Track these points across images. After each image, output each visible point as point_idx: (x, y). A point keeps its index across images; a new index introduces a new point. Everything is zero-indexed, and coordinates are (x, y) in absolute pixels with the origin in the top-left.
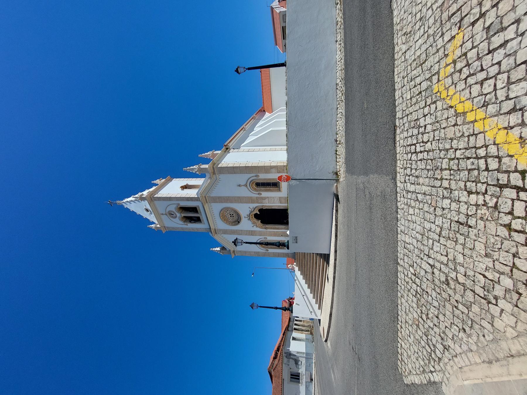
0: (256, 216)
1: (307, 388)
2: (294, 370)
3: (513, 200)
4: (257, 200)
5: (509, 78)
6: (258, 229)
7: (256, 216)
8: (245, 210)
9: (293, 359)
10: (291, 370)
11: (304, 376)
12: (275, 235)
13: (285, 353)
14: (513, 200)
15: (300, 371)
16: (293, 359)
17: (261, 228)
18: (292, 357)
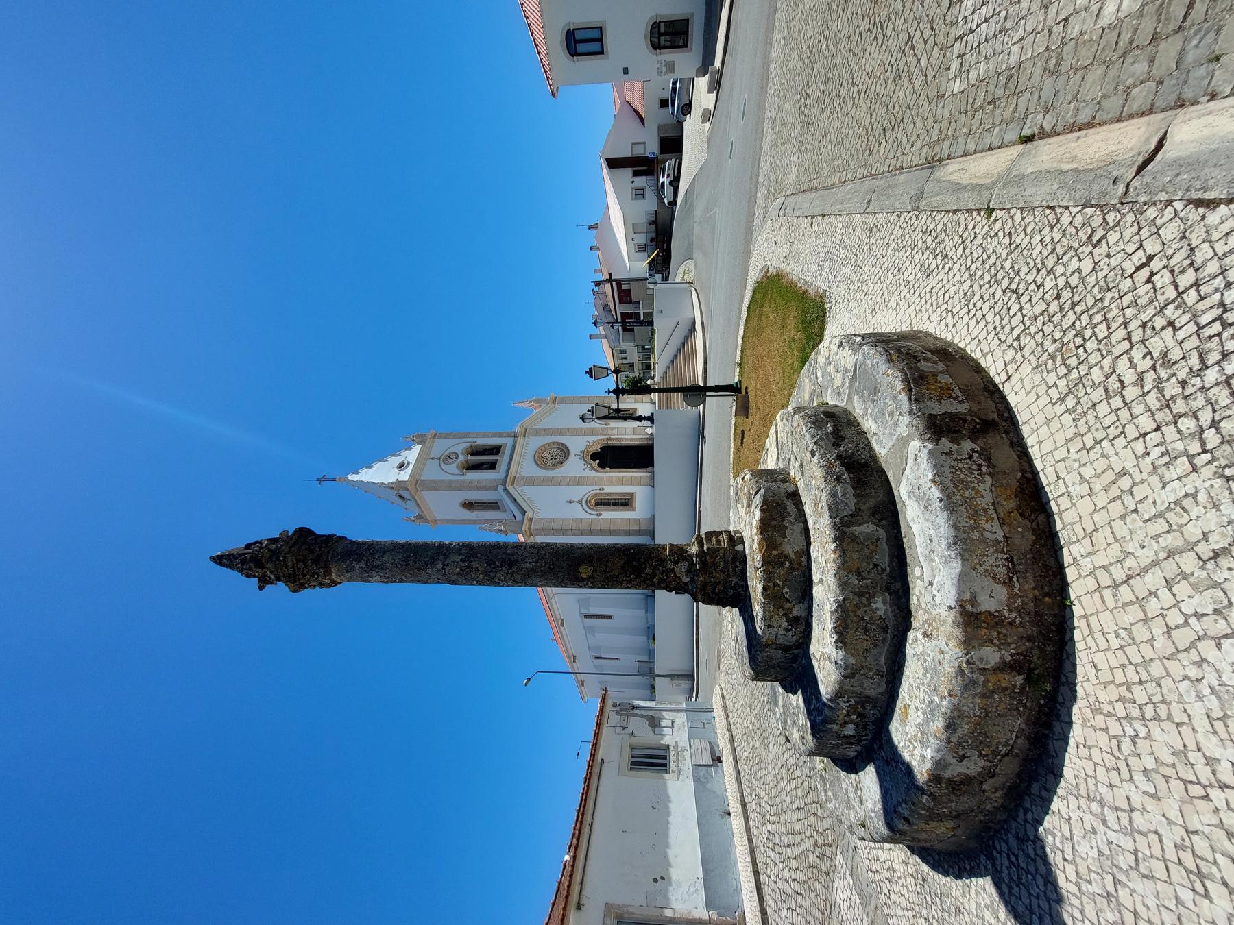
0: (594, 457)
1: (700, 784)
2: (643, 734)
3: (1088, 451)
4: (601, 432)
5: (1191, 782)
6: (593, 473)
7: (594, 457)
8: (579, 444)
9: (641, 716)
10: (634, 741)
11: (687, 754)
12: (621, 482)
13: (615, 705)
14: (1088, 451)
15: (666, 740)
16: (641, 716)
17: (632, 229)
18: (635, 711)
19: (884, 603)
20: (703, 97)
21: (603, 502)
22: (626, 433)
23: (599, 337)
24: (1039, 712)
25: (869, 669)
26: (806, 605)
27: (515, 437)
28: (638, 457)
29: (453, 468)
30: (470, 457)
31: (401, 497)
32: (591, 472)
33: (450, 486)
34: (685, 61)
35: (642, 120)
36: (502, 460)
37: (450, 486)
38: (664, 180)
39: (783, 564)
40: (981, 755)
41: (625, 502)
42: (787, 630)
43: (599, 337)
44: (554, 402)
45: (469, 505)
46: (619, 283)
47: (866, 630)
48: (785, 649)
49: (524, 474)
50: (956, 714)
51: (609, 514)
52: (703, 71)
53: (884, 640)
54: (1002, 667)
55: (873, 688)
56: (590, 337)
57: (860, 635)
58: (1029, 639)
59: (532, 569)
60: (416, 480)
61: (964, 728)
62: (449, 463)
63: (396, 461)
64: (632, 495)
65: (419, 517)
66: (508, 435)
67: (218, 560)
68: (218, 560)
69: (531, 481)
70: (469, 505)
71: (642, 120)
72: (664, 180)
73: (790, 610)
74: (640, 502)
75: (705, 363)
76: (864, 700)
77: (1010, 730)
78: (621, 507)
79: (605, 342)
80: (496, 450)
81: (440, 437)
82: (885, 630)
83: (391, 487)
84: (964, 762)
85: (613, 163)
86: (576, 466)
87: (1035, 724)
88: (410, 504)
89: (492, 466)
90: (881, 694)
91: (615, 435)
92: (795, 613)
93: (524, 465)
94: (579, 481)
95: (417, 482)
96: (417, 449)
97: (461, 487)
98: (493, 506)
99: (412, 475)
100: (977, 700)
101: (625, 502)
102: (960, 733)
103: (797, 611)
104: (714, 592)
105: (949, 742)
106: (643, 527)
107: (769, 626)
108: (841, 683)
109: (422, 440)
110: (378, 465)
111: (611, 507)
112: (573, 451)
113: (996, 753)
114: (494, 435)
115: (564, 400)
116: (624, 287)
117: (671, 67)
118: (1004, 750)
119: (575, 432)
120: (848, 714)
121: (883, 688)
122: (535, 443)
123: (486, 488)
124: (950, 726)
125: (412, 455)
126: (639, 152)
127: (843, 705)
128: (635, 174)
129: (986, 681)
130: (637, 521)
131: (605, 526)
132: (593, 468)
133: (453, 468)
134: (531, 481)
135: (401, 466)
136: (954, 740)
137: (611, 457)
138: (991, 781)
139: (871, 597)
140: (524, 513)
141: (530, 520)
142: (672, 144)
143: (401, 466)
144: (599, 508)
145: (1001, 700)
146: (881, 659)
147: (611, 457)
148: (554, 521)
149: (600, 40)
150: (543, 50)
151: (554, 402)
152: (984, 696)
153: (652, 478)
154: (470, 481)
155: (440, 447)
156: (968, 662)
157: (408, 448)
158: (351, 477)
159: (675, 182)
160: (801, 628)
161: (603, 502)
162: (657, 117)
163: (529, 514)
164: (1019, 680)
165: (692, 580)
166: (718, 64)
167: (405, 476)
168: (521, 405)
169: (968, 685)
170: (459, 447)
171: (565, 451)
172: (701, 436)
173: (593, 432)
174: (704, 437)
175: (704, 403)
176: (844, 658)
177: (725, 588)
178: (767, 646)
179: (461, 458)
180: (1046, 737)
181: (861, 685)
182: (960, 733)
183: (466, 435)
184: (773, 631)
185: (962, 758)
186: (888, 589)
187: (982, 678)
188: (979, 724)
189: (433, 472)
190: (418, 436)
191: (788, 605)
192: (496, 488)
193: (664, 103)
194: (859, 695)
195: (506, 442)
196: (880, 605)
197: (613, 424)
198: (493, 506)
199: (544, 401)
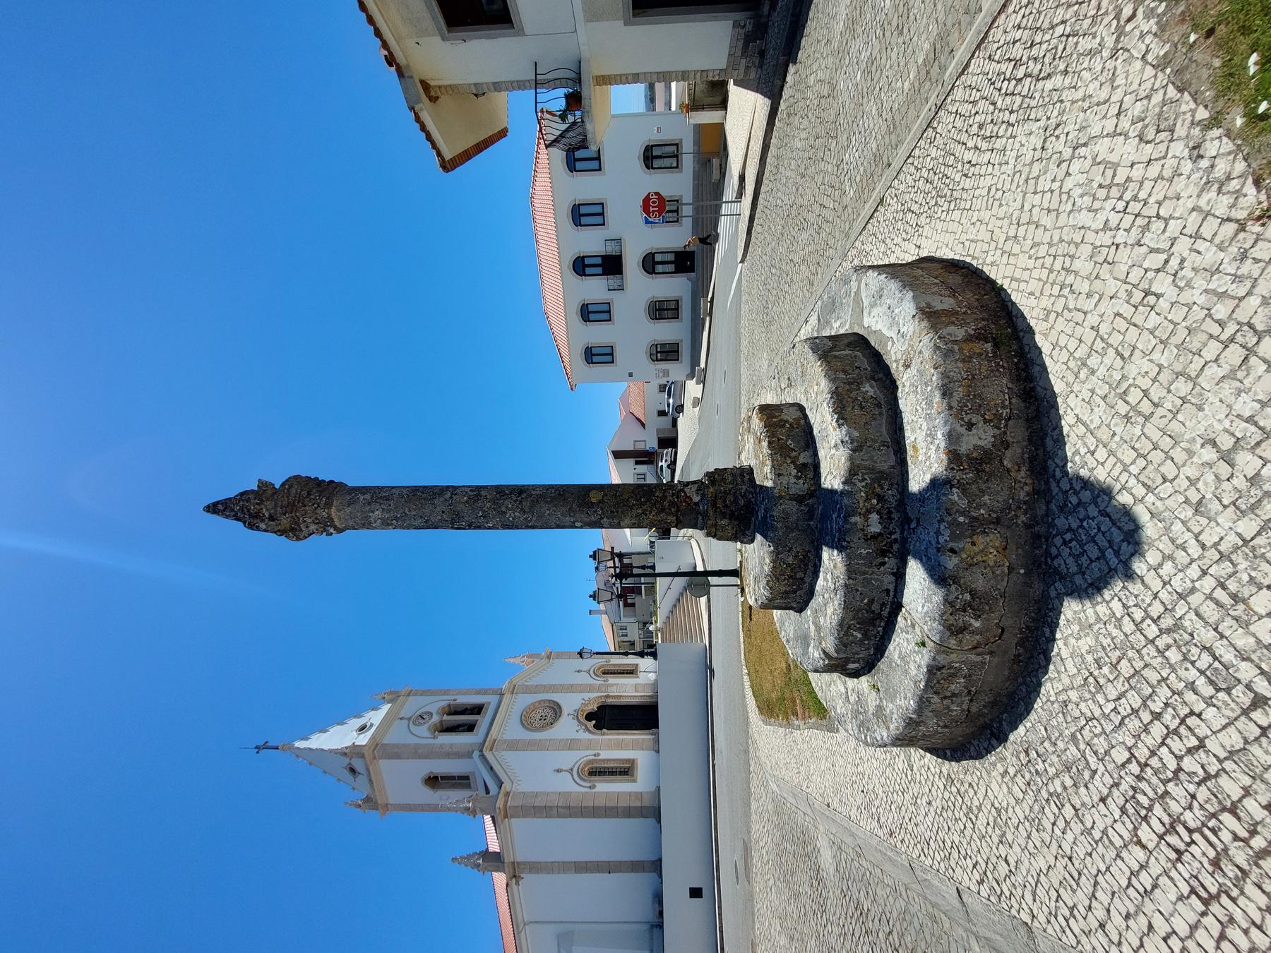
0: (589, 717)
6: (587, 736)
7: (589, 717)
8: (572, 703)
12: (620, 746)
19: (872, 387)
20: (693, 389)
21: (598, 771)
22: (627, 690)
23: (599, 612)
24: (1017, 369)
25: (874, 441)
26: (811, 452)
27: (502, 694)
28: (641, 716)
29: (423, 730)
30: (446, 717)
31: (353, 771)
32: (586, 735)
33: (417, 753)
34: (676, 371)
35: (643, 425)
36: (483, 721)
37: (417, 753)
38: (663, 464)
39: (784, 426)
40: (986, 421)
41: (624, 771)
42: (798, 478)
43: (599, 612)
44: (549, 657)
45: (433, 781)
46: (621, 556)
47: (862, 408)
48: (799, 499)
49: (505, 737)
50: (946, 381)
51: (608, 788)
52: (691, 376)
53: (880, 414)
54: (969, 339)
55: (885, 462)
56: (590, 612)
57: (857, 411)
58: (983, 319)
59: (541, 496)
60: (375, 744)
61: (959, 393)
62: (420, 724)
63: (358, 722)
64: (633, 762)
65: (368, 800)
66: (494, 692)
67: (213, 508)
68: (213, 508)
69: (514, 746)
70: (433, 781)
71: (643, 425)
72: (663, 464)
73: (797, 457)
74: (642, 771)
75: (710, 629)
76: (880, 477)
77: (999, 390)
78: (619, 777)
79: (604, 617)
80: (478, 709)
81: (416, 694)
82: (879, 406)
83: (343, 753)
84: (974, 431)
85: (618, 455)
86: (568, 728)
87: (1018, 380)
88: (362, 780)
89: (470, 728)
90: (893, 467)
91: (614, 692)
92: (801, 460)
93: (506, 724)
94: (571, 745)
95: (380, 749)
96: (386, 708)
97: (429, 754)
98: (462, 781)
99: (373, 738)
100: (960, 365)
101: (624, 771)
102: (956, 396)
103: (804, 458)
104: (726, 506)
105: (950, 408)
106: (647, 802)
107: (779, 475)
108: (851, 459)
109: (393, 697)
110: (336, 729)
111: (607, 777)
112: (565, 711)
113: (998, 417)
114: (478, 692)
115: (560, 655)
116: (626, 561)
117: (666, 373)
118: (1005, 412)
119: (571, 689)
120: (868, 499)
121: (892, 460)
122: (525, 700)
123: (459, 755)
124: (946, 393)
125: (376, 717)
126: (641, 447)
127: (860, 485)
128: (637, 463)
129: (961, 349)
130: (639, 795)
131: (600, 802)
132: (587, 729)
133: (423, 730)
134: (514, 746)
135: (362, 729)
136: (954, 404)
137: (610, 717)
138: (1008, 453)
139: (859, 385)
140: (500, 784)
141: (507, 794)
142: (669, 442)
143: (362, 729)
144: (593, 778)
145: (980, 365)
146: (881, 430)
147: (610, 717)
148: (536, 795)
149: (612, 354)
150: (566, 359)
151: (549, 657)
152: (963, 361)
153: (657, 741)
154: (441, 746)
155: (413, 706)
156: (940, 338)
157: (375, 708)
158: (300, 744)
159: (674, 462)
160: (811, 475)
161: (598, 771)
162: (656, 425)
163: (507, 786)
164: (989, 346)
165: (703, 496)
166: (703, 365)
167: (363, 740)
168: (512, 660)
169: (947, 354)
170: (435, 705)
171: (556, 710)
172: (709, 670)
173: (590, 689)
174: (712, 671)
175: (708, 593)
176: (848, 433)
177: (736, 498)
178: (781, 497)
179: (436, 719)
180: (1033, 389)
181: (871, 458)
182: (956, 396)
183: (446, 692)
184: (784, 480)
185: (970, 426)
186: (873, 378)
187: (956, 348)
188: (970, 386)
189: (399, 735)
190: (391, 693)
191: (794, 454)
192: (469, 755)
193: (662, 413)
194: (872, 470)
195: (491, 700)
196: (869, 389)
197: (612, 680)
198: (462, 781)
199: (537, 656)
